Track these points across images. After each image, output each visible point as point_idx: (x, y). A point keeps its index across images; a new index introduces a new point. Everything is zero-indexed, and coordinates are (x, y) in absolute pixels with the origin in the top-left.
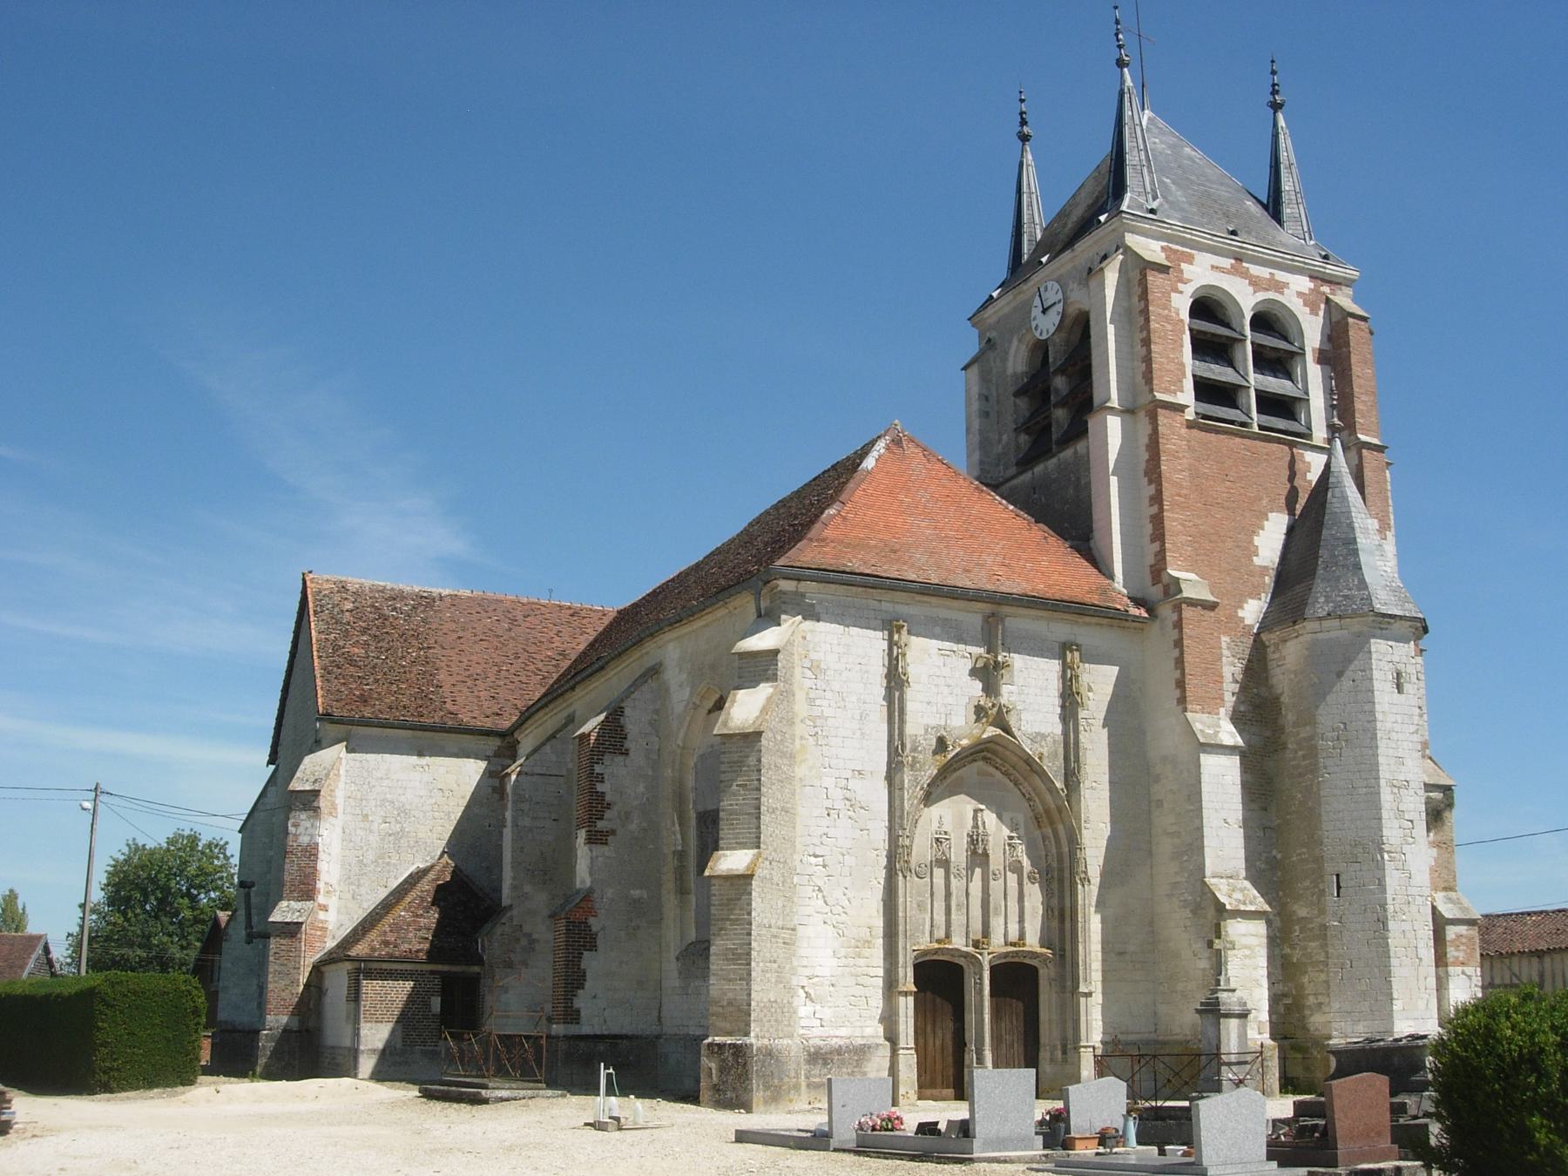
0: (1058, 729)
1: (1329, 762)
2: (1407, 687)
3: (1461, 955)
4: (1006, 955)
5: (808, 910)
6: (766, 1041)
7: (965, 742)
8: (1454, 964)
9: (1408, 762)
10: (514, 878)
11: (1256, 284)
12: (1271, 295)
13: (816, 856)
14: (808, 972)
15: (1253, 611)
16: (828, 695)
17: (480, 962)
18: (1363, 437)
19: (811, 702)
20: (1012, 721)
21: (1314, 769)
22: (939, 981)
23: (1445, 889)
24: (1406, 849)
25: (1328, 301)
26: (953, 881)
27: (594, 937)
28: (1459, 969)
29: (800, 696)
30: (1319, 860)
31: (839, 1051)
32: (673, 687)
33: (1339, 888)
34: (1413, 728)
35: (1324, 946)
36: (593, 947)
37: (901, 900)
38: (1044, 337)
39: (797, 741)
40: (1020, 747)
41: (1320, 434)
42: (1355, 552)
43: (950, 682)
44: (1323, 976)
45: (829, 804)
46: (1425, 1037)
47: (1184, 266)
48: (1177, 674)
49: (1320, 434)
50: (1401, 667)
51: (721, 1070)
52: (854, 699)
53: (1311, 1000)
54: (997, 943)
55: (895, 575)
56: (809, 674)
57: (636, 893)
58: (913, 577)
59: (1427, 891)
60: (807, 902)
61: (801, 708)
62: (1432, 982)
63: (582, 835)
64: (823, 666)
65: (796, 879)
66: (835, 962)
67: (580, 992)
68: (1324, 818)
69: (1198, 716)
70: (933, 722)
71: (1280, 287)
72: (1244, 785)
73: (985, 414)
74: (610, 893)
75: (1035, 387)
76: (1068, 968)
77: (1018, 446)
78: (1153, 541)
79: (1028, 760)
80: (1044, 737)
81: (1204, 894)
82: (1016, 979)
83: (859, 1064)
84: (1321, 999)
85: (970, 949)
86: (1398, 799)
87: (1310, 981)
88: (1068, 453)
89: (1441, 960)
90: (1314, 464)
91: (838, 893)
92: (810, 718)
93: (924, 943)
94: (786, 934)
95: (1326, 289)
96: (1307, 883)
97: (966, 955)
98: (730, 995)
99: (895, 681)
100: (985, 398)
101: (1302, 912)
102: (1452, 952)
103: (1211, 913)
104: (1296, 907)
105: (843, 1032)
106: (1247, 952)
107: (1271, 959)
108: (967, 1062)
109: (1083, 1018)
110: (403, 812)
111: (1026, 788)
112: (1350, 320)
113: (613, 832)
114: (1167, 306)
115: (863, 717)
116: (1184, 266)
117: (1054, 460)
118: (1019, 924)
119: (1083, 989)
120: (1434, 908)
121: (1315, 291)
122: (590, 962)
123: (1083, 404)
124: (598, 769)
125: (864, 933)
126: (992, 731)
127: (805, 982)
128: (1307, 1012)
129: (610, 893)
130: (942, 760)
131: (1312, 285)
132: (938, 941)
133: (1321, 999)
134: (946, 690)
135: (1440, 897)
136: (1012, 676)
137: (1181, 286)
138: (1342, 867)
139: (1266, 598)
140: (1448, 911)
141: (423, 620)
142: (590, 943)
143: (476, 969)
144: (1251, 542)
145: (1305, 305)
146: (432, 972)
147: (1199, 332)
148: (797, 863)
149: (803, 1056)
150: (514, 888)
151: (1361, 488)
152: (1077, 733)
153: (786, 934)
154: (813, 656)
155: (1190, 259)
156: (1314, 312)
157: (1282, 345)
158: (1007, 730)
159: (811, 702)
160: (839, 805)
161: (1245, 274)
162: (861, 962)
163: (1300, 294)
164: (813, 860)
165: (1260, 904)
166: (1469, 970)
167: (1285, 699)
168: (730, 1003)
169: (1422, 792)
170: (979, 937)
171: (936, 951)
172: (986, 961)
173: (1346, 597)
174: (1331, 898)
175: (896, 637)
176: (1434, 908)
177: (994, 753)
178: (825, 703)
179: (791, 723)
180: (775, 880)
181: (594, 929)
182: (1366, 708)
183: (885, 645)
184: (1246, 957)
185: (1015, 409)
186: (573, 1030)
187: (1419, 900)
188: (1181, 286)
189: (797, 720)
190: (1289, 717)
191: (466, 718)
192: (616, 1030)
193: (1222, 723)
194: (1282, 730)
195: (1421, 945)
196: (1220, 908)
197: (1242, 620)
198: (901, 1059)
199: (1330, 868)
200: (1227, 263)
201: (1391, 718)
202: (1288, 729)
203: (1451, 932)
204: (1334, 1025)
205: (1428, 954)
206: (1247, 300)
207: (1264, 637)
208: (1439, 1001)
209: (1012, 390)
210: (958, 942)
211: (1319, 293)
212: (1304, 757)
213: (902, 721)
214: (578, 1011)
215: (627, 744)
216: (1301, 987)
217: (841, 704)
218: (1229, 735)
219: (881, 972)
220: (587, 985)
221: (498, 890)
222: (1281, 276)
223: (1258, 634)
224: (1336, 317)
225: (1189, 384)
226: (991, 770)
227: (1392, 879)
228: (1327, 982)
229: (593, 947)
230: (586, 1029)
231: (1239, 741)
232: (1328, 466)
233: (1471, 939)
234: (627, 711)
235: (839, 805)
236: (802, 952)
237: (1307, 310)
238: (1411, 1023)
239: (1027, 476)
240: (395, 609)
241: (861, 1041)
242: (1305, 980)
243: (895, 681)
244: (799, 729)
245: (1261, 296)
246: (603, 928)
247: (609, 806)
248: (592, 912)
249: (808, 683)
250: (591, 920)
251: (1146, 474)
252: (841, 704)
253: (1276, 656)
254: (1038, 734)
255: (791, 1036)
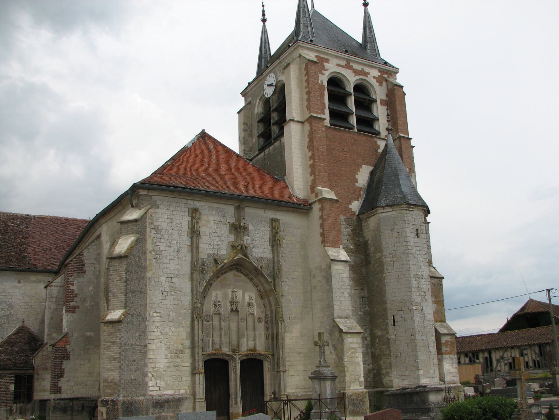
0: (270, 256)
1: (389, 268)
2: (420, 235)
3: (448, 349)
4: (247, 355)
5: (153, 337)
6: (128, 399)
7: (226, 261)
8: (445, 354)
9: (423, 267)
10: (48, 331)
11: (356, 72)
12: (362, 77)
13: (157, 312)
14: (153, 365)
15: (355, 206)
16: (162, 240)
17: (33, 368)
18: (401, 135)
19: (154, 244)
20: (249, 252)
21: (382, 272)
22: (215, 370)
23: (441, 321)
24: (423, 304)
25: (386, 80)
26: (223, 323)
27: (68, 354)
28: (447, 356)
29: (149, 241)
30: (385, 310)
31: (168, 401)
32: (104, 243)
33: (394, 321)
34: (424, 253)
35: (389, 347)
36: (68, 358)
37: (197, 332)
38: (269, 96)
39: (148, 262)
40: (251, 263)
41: (384, 133)
42: (398, 179)
43: (220, 235)
44: (389, 360)
45: (162, 289)
46: (425, 386)
47: (325, 64)
48: (321, 230)
49: (384, 133)
50: (418, 227)
51: (107, 413)
52: (175, 242)
53: (384, 371)
54: (244, 349)
55: (194, 188)
56: (153, 231)
57: (88, 334)
58: (202, 189)
59: (432, 322)
60: (152, 333)
61: (149, 246)
62: (436, 361)
63: (64, 308)
64: (160, 228)
65: (147, 323)
66: (166, 361)
67: (62, 379)
68: (387, 292)
69: (330, 248)
70: (211, 252)
71: (366, 74)
72: (352, 279)
73: (245, 130)
74: (76, 335)
75: (265, 120)
76: (276, 360)
77: (259, 144)
78: (311, 175)
79: (256, 269)
80: (263, 259)
81: (334, 327)
82: (253, 367)
83: (177, 407)
84: (388, 370)
85: (231, 353)
86: (419, 283)
87: (383, 362)
88: (277, 144)
89: (439, 351)
90: (382, 144)
91: (167, 330)
92: (154, 250)
93: (209, 350)
94: (141, 348)
95: (385, 76)
96: (381, 320)
97: (228, 355)
98: (111, 377)
99: (194, 233)
100: (245, 124)
101: (379, 333)
102: (444, 349)
103: (337, 333)
104: (376, 331)
105: (170, 392)
106: (353, 351)
107: (365, 354)
108: (230, 404)
109: (282, 382)
110: (11, 306)
111: (256, 281)
112: (396, 87)
113: (78, 307)
114: (317, 78)
115: (179, 250)
116: (325, 64)
117: (272, 146)
118: (255, 341)
119: (282, 369)
120: (436, 329)
121: (381, 76)
122: (66, 365)
123: (282, 121)
124: (71, 279)
125: (180, 347)
126: (240, 256)
127: (151, 370)
128: (383, 376)
129: (76, 335)
130: (215, 269)
131: (379, 74)
132: (215, 350)
133: (388, 370)
134: (218, 238)
135: (438, 325)
136: (248, 233)
137: (323, 72)
138: (395, 313)
139: (361, 200)
140: (442, 331)
141: (26, 227)
142: (66, 356)
143: (31, 371)
144: (355, 177)
145: (377, 82)
146: (11, 374)
147: (332, 91)
148: (148, 316)
149: (150, 404)
150: (48, 335)
151: (401, 155)
152: (278, 257)
153: (141, 348)
154: (156, 223)
155: (327, 61)
156: (381, 84)
157: (367, 98)
158: (246, 255)
159: (154, 244)
160: (167, 289)
161: (350, 68)
162: (179, 360)
163: (374, 77)
164: (155, 314)
165: (358, 329)
166: (452, 356)
167: (369, 242)
168: (111, 382)
169: (429, 280)
170: (235, 347)
171: (215, 354)
172: (237, 357)
173: (394, 197)
174: (391, 328)
175: (194, 215)
176: (436, 329)
177: (241, 266)
178: (161, 244)
179: (145, 253)
180: (135, 323)
181: (69, 350)
182: (404, 244)
183: (190, 219)
184: (353, 352)
185: (257, 129)
186: (58, 396)
187: (429, 326)
188: (323, 72)
189: (148, 252)
190: (372, 249)
191: (39, 266)
192: (79, 395)
193: (341, 251)
194: (369, 255)
195: (431, 345)
196: (341, 331)
197: (351, 209)
198: (197, 404)
199: (390, 314)
200: (343, 63)
201: (415, 248)
202: (372, 255)
203: (444, 339)
204: (394, 382)
205: (434, 349)
206: (351, 80)
207: (361, 216)
208: (439, 369)
209: (257, 120)
210: (225, 350)
211: (383, 77)
212: (378, 267)
213: (198, 252)
214: (60, 388)
215: (85, 268)
216: (379, 366)
217: (169, 244)
218: (343, 255)
219: (188, 364)
220: (65, 375)
221: (44, 337)
222: (366, 69)
223: (358, 215)
224: (390, 87)
225: (327, 111)
226: (239, 274)
227: (417, 318)
228: (390, 363)
229: (68, 358)
230: (64, 396)
231: (348, 258)
232: (386, 145)
233: (452, 342)
234: (85, 254)
235: (167, 289)
236: (150, 356)
237: (378, 84)
238: (428, 380)
239: (262, 155)
240: (13, 223)
241: (178, 396)
242: (382, 362)
243: (194, 233)
244: (149, 256)
245: (358, 77)
246: (73, 350)
247: (76, 296)
248: (67, 343)
249: (153, 235)
250: (67, 346)
251: (308, 147)
252: (169, 244)
253: (366, 224)
254: (260, 258)
255: (144, 395)
